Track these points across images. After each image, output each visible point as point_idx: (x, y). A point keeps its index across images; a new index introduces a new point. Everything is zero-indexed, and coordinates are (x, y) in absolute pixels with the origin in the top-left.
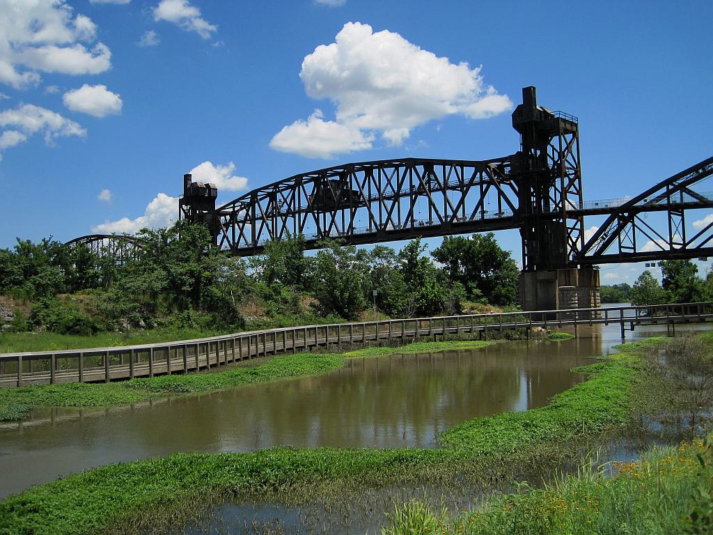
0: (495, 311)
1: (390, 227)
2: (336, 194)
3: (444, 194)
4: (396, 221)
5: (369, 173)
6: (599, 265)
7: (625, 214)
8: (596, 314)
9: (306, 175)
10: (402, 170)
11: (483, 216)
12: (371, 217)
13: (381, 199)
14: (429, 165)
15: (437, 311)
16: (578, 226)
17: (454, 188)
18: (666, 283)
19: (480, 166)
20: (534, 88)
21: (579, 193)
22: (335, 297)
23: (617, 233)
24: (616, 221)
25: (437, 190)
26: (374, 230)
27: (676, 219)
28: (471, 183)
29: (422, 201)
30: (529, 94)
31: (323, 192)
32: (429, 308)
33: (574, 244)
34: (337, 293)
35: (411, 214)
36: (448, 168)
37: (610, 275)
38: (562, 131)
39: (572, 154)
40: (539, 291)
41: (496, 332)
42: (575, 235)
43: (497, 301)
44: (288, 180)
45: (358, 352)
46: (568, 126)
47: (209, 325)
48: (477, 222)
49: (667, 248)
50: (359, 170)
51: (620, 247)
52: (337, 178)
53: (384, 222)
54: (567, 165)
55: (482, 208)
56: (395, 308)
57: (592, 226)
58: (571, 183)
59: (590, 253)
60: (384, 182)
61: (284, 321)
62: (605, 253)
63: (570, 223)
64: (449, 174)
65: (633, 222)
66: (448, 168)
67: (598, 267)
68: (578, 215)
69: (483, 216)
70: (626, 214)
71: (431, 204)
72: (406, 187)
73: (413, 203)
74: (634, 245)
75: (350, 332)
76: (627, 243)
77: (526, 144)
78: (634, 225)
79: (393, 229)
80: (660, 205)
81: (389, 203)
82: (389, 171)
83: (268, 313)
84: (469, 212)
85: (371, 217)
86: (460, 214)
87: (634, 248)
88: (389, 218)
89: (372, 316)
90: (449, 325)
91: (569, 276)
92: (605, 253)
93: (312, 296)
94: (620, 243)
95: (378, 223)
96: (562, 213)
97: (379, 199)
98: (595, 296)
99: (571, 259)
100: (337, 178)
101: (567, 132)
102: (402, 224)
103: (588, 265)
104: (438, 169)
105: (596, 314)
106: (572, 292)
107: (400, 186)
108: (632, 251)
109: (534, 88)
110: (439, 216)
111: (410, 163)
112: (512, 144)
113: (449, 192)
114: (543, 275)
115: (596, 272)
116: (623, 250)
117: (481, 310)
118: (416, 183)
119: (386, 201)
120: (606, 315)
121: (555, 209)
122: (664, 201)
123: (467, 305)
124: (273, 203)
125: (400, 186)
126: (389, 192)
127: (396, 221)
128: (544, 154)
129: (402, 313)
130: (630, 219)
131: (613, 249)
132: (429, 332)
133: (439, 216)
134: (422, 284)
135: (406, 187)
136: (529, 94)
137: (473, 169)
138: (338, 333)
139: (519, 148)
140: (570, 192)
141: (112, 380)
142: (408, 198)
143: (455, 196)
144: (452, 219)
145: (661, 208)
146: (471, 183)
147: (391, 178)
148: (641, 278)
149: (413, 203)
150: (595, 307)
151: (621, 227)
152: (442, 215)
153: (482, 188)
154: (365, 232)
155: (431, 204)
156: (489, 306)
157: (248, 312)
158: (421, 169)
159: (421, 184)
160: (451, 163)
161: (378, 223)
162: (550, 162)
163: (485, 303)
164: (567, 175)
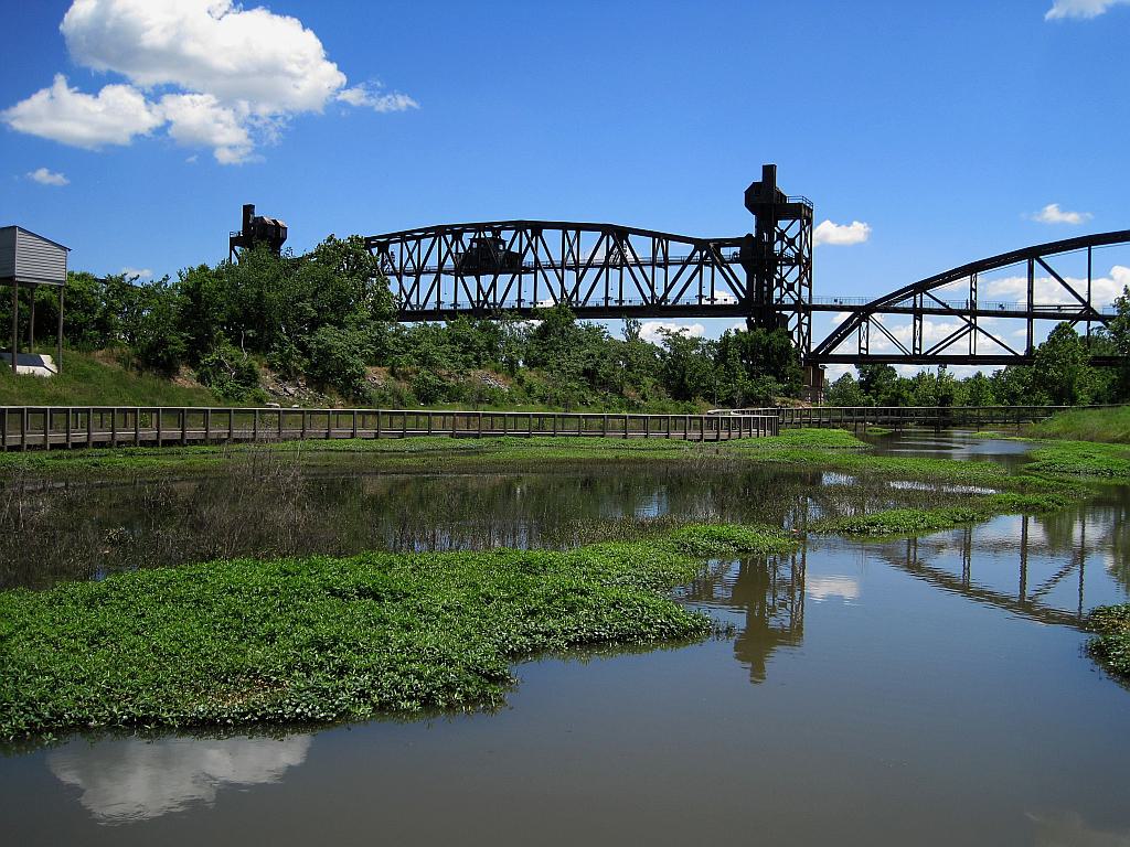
3: (400, 281)
7: (862, 313)
9: (374, 238)
14: (620, 234)
17: (569, 268)
19: (699, 244)
25: (391, 274)
30: (769, 171)
62: (833, 352)
69: (439, 306)
72: (433, 263)
82: (411, 244)
92: (833, 352)
102: (421, 302)
136: (248, 210)
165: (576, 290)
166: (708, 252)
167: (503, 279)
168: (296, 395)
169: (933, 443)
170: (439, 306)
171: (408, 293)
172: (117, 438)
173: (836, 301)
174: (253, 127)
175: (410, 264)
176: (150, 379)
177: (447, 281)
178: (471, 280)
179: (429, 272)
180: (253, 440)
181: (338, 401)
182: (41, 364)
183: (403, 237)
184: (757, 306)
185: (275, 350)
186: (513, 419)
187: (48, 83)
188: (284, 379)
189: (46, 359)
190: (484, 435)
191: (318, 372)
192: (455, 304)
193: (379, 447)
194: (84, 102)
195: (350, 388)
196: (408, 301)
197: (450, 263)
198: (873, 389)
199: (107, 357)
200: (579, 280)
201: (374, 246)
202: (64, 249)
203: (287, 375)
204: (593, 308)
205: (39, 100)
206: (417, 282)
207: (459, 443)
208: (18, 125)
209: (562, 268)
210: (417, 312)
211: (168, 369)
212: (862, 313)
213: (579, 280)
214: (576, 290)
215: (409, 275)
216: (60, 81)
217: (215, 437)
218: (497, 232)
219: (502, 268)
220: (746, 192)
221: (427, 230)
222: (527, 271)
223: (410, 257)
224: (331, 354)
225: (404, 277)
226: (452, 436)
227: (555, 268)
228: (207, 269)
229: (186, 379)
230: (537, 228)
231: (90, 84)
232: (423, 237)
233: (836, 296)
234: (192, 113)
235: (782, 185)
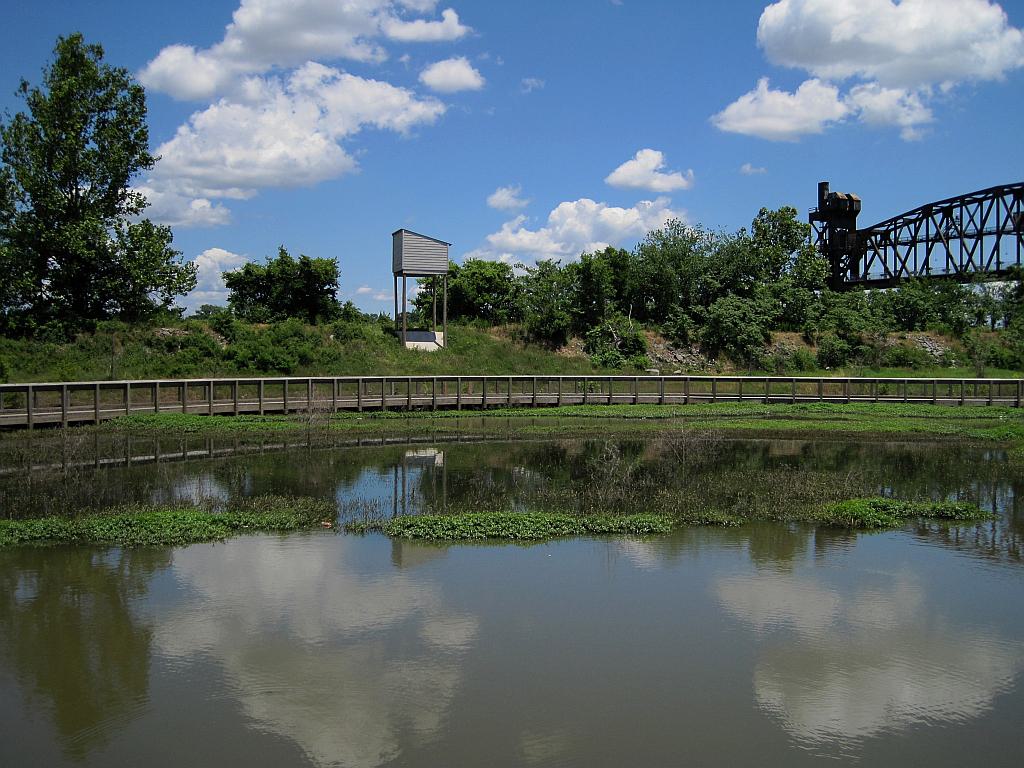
3: (895, 249)
4: (977, 262)
5: (947, 213)
9: (936, 204)
10: (986, 204)
11: (998, 267)
12: (949, 256)
13: (962, 235)
25: (955, 237)
35: (926, 262)
39: (969, 213)
44: (912, 213)
45: (743, 426)
50: (1008, 193)
53: (964, 263)
55: (928, 266)
73: (929, 251)
81: (970, 243)
82: (972, 207)
85: (949, 256)
86: (910, 265)
88: (970, 260)
102: (985, 263)
107: (983, 222)
110: (955, 265)
113: (898, 247)
120: (714, 391)
125: (983, 222)
126: (971, 229)
127: (977, 262)
132: (584, 399)
133: (955, 265)
135: (991, 224)
136: (823, 187)
138: (233, 396)
141: (437, 441)
142: (925, 244)
149: (929, 251)
150: (289, 390)
152: (958, 264)
153: (927, 245)
161: (958, 264)
168: (686, 362)
171: (970, 251)
172: (412, 404)
174: (936, 105)
176: (534, 352)
179: (990, 233)
180: (407, 407)
181: (728, 365)
182: (433, 339)
183: (963, 201)
185: (670, 320)
186: (896, 385)
187: (752, 86)
188: (677, 346)
189: (439, 336)
190: (798, 401)
191: (714, 339)
193: (688, 412)
194: (779, 98)
195: (744, 356)
197: (1010, 225)
199: (498, 333)
201: (938, 212)
202: (446, 244)
203: (681, 341)
205: (744, 103)
207: (768, 409)
208: (724, 127)
211: (557, 339)
216: (763, 83)
217: (390, 404)
221: (986, 192)
223: (972, 219)
224: (722, 322)
225: (898, 247)
226: (764, 402)
228: (613, 250)
229: (573, 348)
231: (789, 82)
232: (985, 199)
234: (880, 101)
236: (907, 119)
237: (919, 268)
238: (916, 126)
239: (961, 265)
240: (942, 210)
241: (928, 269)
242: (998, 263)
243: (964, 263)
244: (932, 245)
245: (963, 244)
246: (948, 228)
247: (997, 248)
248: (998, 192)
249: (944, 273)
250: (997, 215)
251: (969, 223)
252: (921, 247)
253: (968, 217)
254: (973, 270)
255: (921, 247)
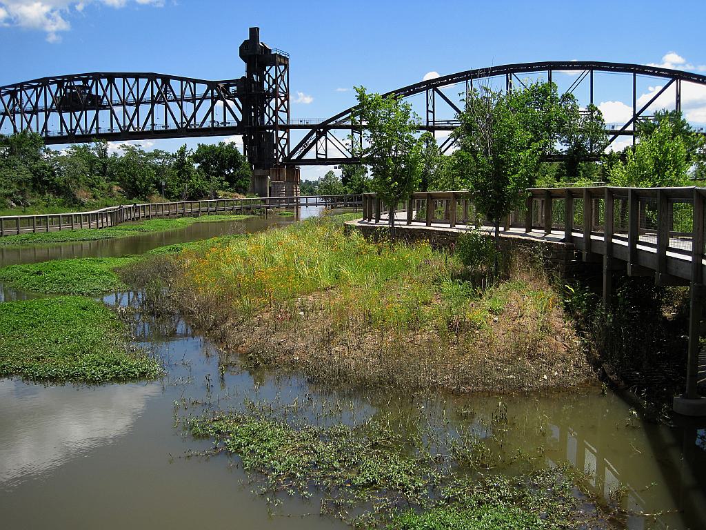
0: (241, 197)
1: (78, 132)
2: (82, 98)
5: (13, 95)
6: (300, 166)
7: (321, 130)
8: (297, 200)
9: (4, 88)
11: (97, 131)
13: (23, 112)
14: (166, 79)
15: (201, 197)
16: (286, 136)
17: (188, 100)
18: (345, 180)
19: (212, 85)
20: (258, 29)
21: (287, 111)
22: (137, 186)
23: (315, 142)
24: (315, 134)
25: (173, 101)
26: (65, 134)
27: (357, 136)
28: (204, 98)
29: (55, 117)
30: (254, 32)
31: (70, 96)
32: (197, 195)
33: (283, 150)
34: (138, 183)
35: (45, 126)
36: (184, 83)
37: (309, 174)
38: (277, 64)
39: (27, 95)
40: (256, 184)
41: (248, 210)
42: (283, 142)
43: (242, 190)
46: (282, 60)
47: (63, 204)
48: (148, 132)
49: (350, 156)
50: (52, 83)
51: (317, 154)
52: (81, 83)
53: (74, 128)
54: (280, 90)
55: (46, 130)
56: (173, 194)
57: (297, 136)
58: (282, 102)
59: (294, 157)
60: (25, 99)
61: (109, 202)
62: (304, 158)
63: (281, 133)
64: (185, 89)
65: (326, 136)
66: (184, 83)
67: (299, 168)
68: (286, 128)
69: (153, 128)
70: (322, 130)
71: (62, 121)
72: (148, 96)
73: (47, 117)
74: (326, 152)
75: (17, 225)
76: (321, 151)
77: (250, 71)
78: (326, 138)
79: (81, 133)
80: (346, 126)
81: (28, 116)
82: (29, 92)
83: (94, 197)
84: (199, 119)
86: (135, 123)
87: (326, 155)
88: (78, 124)
89: (158, 199)
90: (211, 206)
91: (279, 174)
92: (304, 158)
93: (117, 185)
94: (317, 151)
95: (69, 128)
96: (276, 127)
97: (21, 113)
98: (296, 189)
99: (280, 160)
100: (81, 83)
101: (281, 64)
102: (141, 126)
103: (292, 165)
104: (175, 85)
105: (297, 200)
106: (281, 185)
108: (324, 157)
109: (258, 29)
110: (119, 125)
111: (152, 77)
112: (238, 69)
114: (259, 172)
115: (298, 171)
116: (319, 156)
117: (230, 197)
118: (156, 91)
119: (26, 115)
121: (269, 122)
122: (349, 123)
123: (221, 193)
124: (14, 101)
128: (263, 78)
129: (179, 197)
130: (324, 133)
131: (311, 155)
133: (119, 125)
134: (190, 178)
136: (254, 32)
137: (206, 86)
139: (245, 74)
140: (281, 111)
143: (189, 108)
144: (186, 126)
145: (347, 127)
146: (204, 98)
147: (31, 96)
148: (327, 177)
149: (47, 117)
151: (318, 139)
154: (57, 135)
155: (62, 121)
156: (236, 194)
157: (83, 195)
158: (159, 81)
159: (159, 92)
160: (188, 80)
161: (69, 128)
162: (266, 86)
163: (233, 192)
164: (280, 97)
165: (194, 116)
166: (218, 90)
167: (91, 114)
169: (593, 219)
170: (153, 128)
173: (301, 121)
175: (29, 105)
177: (55, 117)
178: (66, 116)
179: (145, 103)
183: (125, 76)
184: (253, 128)
192: (225, 122)
196: (131, 124)
198: (349, 181)
200: (196, 109)
204: (206, 128)
206: (137, 111)
209: (181, 101)
210: (138, 133)
212: (321, 130)
213: (196, 109)
214: (194, 116)
215: (131, 105)
218: (85, 81)
219: (86, 106)
220: (241, 48)
222: (104, 108)
223: (29, 100)
227: (177, 101)
230: (111, 77)
233: (301, 118)
235: (265, 40)
236: (51, 28)
237: (40, 131)
238: (57, 33)
239: (124, 126)
240: (9, 92)
241: (47, 132)
242: (98, 128)
243: (74, 128)
244: (49, 114)
245: (125, 111)
246: (14, 105)
247: (96, 118)
248: (45, 82)
249: (60, 135)
250: (48, 98)
251: (129, 94)
252: (42, 115)
253: (28, 98)
254: (81, 133)
255: (42, 115)
